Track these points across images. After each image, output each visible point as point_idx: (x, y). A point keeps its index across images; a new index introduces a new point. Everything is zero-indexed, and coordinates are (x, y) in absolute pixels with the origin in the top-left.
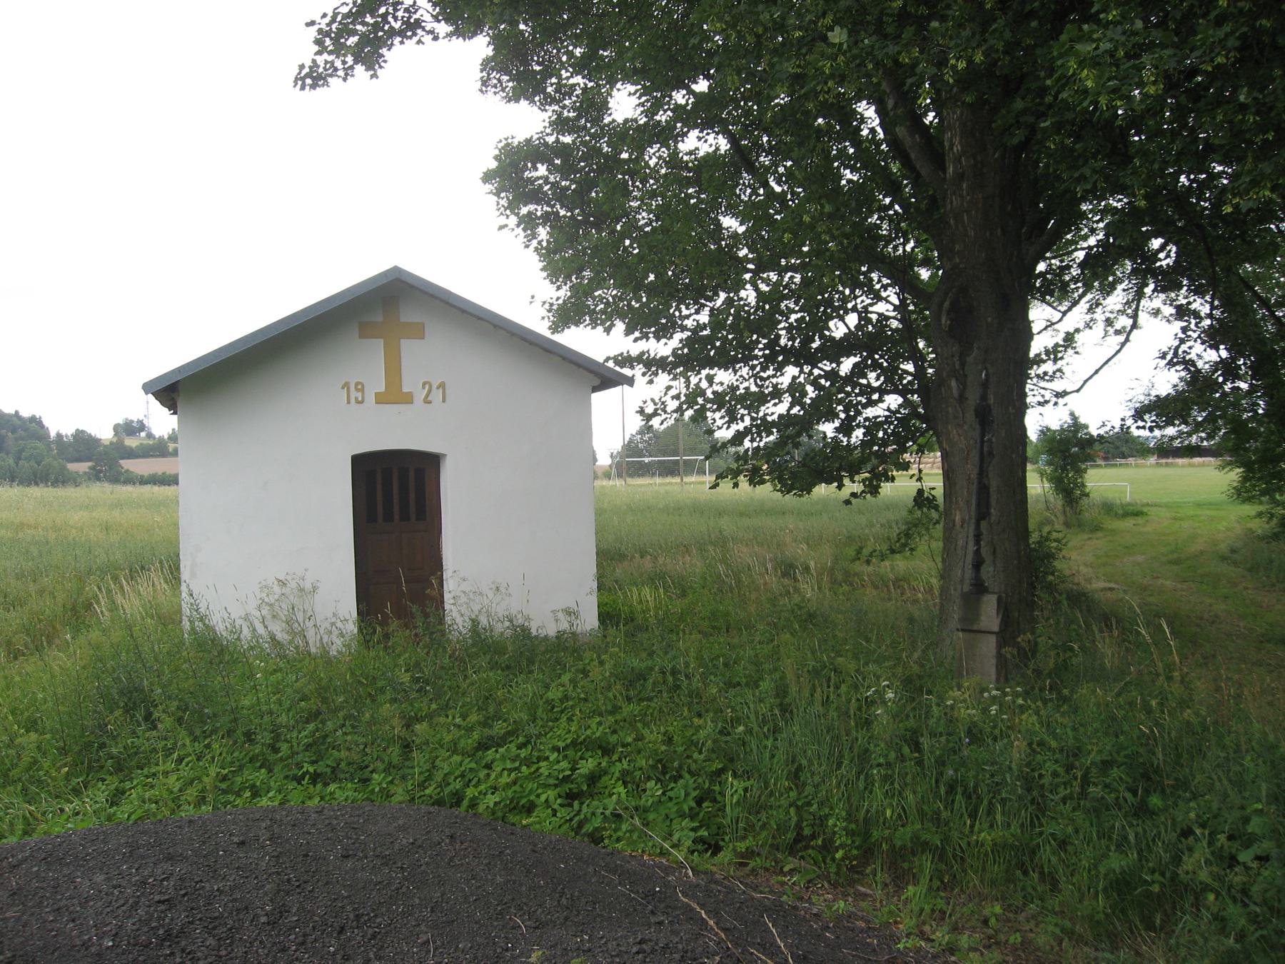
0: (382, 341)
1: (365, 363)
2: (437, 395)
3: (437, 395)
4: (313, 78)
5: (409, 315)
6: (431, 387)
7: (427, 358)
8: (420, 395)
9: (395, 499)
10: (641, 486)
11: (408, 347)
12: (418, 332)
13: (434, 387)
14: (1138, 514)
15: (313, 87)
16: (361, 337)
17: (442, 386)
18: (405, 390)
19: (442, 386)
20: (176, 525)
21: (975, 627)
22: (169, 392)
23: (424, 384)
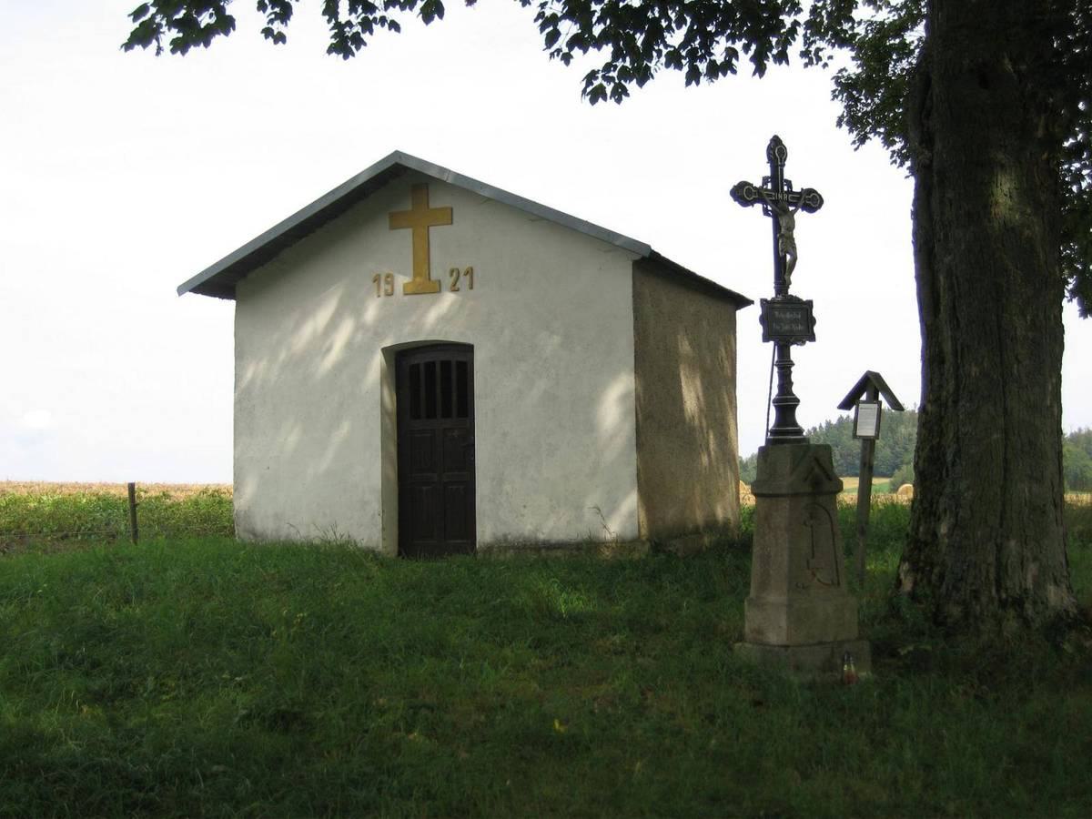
0: (410, 230)
1: (390, 250)
2: (464, 280)
3: (464, 280)
4: (128, 46)
5: (438, 201)
6: (459, 273)
7: (452, 242)
8: (448, 281)
9: (431, 394)
10: (708, 444)
11: (437, 234)
12: (448, 217)
13: (462, 275)
14: (830, 479)
15: (180, 46)
16: (393, 228)
17: (470, 272)
18: (771, 344)
19: (470, 272)
20: (240, 354)
21: (128, 505)
22: (846, 404)
23: (452, 271)
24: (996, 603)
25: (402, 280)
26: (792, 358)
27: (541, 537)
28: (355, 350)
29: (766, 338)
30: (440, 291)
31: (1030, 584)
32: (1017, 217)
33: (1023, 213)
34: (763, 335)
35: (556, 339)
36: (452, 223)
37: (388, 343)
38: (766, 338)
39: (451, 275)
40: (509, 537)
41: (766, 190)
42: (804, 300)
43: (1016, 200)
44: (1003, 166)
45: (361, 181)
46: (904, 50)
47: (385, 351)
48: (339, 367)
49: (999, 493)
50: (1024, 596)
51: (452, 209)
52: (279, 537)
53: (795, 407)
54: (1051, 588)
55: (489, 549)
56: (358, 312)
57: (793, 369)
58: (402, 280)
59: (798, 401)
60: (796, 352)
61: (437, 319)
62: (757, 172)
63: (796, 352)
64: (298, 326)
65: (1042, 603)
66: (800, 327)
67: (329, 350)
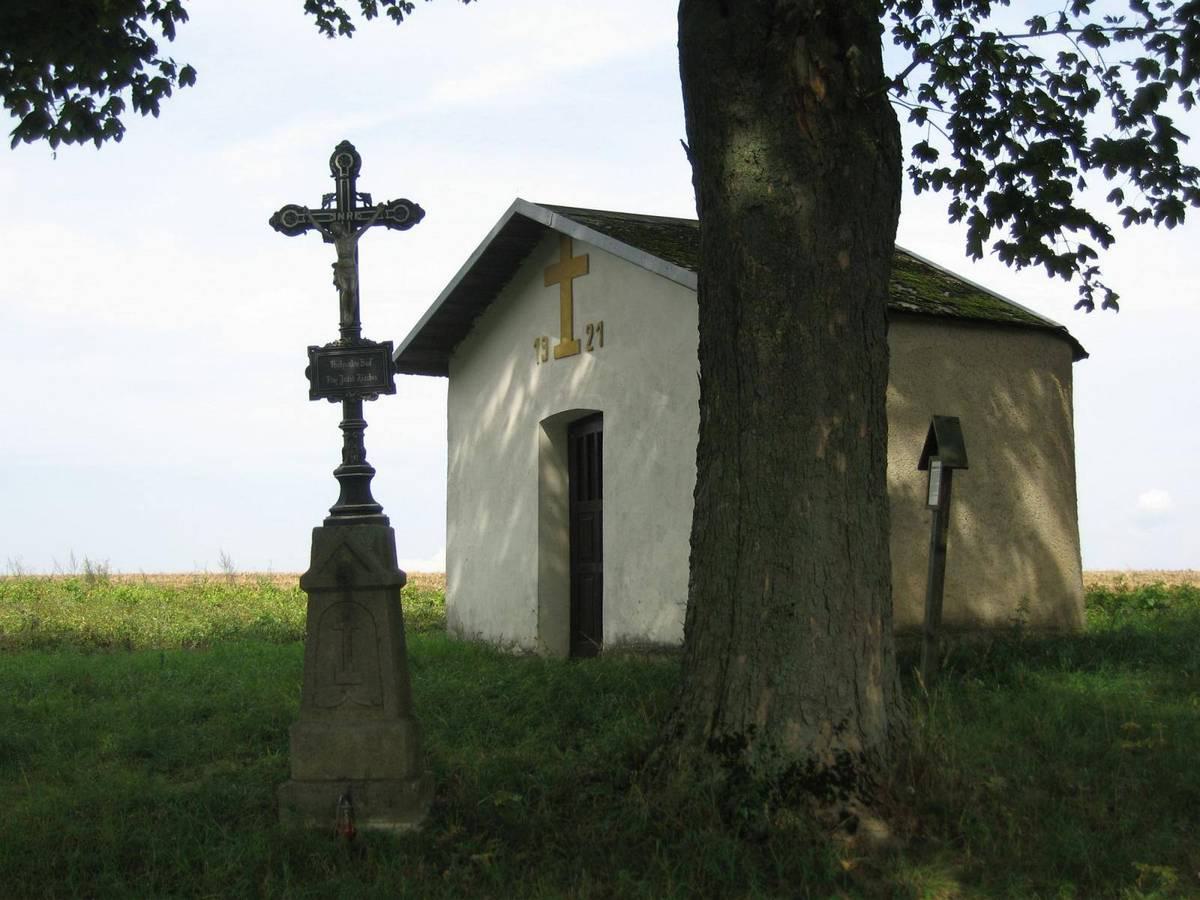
1: (540, 312)
19: (601, 328)
24: (704, 745)
25: (555, 342)
26: (365, 418)
27: (652, 638)
28: (525, 426)
29: (390, 389)
30: (580, 352)
31: (761, 720)
32: (769, 190)
33: (777, 183)
34: (311, 392)
35: (665, 399)
36: (588, 272)
37: (545, 415)
38: (390, 389)
39: (588, 333)
40: (628, 638)
41: (329, 210)
42: (379, 341)
43: (765, 166)
44: (741, 122)
45: (496, 233)
46: (133, 31)
47: (547, 424)
48: (514, 442)
49: (726, 587)
50: (748, 736)
51: (588, 256)
52: (638, 635)
53: (370, 478)
54: (793, 726)
55: (612, 651)
56: (526, 381)
57: (365, 431)
58: (555, 342)
59: (372, 471)
60: (369, 408)
61: (581, 382)
62: (377, 184)
63: (369, 408)
64: (486, 401)
65: (773, 748)
66: (371, 378)
67: (506, 425)
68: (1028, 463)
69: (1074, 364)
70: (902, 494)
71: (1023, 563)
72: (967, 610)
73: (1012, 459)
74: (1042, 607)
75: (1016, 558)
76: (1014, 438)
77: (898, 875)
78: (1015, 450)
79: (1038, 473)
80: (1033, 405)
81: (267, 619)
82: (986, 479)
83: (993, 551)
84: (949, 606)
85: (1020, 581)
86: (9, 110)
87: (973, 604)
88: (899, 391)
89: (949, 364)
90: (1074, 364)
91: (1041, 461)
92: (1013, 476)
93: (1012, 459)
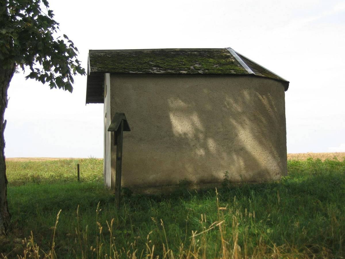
68: (242, 124)
69: (285, 92)
70: (183, 136)
71: (238, 159)
72: (212, 176)
73: (234, 122)
74: (248, 175)
75: (235, 157)
76: (236, 116)
77: (250, 244)
78: (235, 119)
79: (246, 126)
80: (244, 102)
81: (61, 176)
82: (222, 130)
83: (224, 155)
84: (81, 176)
85: (237, 165)
86: (38, 80)
87: (215, 174)
88: (183, 101)
89: (205, 91)
90: (285, 92)
91: (247, 122)
92: (234, 128)
93: (234, 122)
